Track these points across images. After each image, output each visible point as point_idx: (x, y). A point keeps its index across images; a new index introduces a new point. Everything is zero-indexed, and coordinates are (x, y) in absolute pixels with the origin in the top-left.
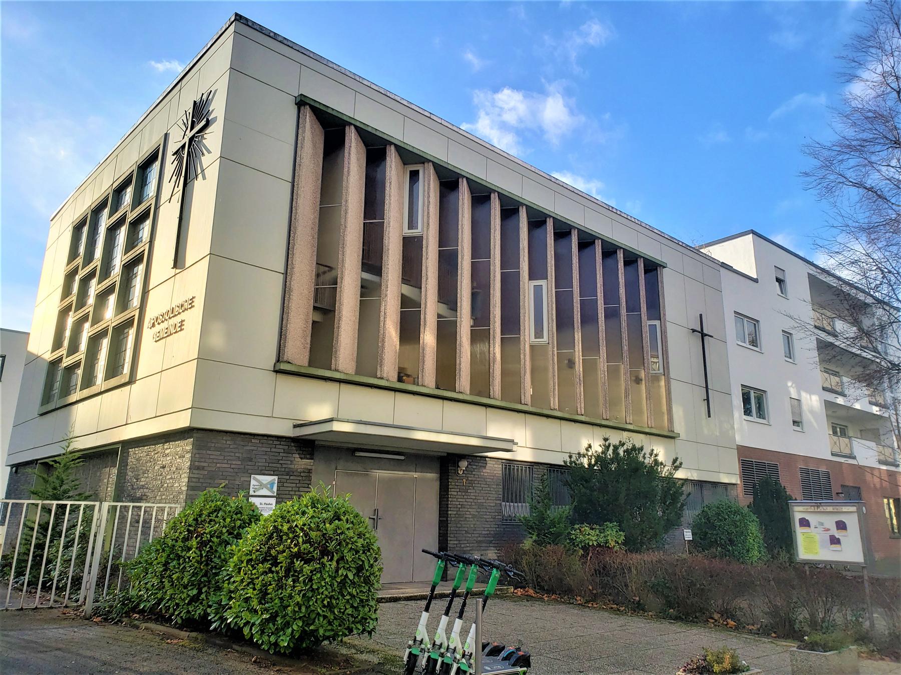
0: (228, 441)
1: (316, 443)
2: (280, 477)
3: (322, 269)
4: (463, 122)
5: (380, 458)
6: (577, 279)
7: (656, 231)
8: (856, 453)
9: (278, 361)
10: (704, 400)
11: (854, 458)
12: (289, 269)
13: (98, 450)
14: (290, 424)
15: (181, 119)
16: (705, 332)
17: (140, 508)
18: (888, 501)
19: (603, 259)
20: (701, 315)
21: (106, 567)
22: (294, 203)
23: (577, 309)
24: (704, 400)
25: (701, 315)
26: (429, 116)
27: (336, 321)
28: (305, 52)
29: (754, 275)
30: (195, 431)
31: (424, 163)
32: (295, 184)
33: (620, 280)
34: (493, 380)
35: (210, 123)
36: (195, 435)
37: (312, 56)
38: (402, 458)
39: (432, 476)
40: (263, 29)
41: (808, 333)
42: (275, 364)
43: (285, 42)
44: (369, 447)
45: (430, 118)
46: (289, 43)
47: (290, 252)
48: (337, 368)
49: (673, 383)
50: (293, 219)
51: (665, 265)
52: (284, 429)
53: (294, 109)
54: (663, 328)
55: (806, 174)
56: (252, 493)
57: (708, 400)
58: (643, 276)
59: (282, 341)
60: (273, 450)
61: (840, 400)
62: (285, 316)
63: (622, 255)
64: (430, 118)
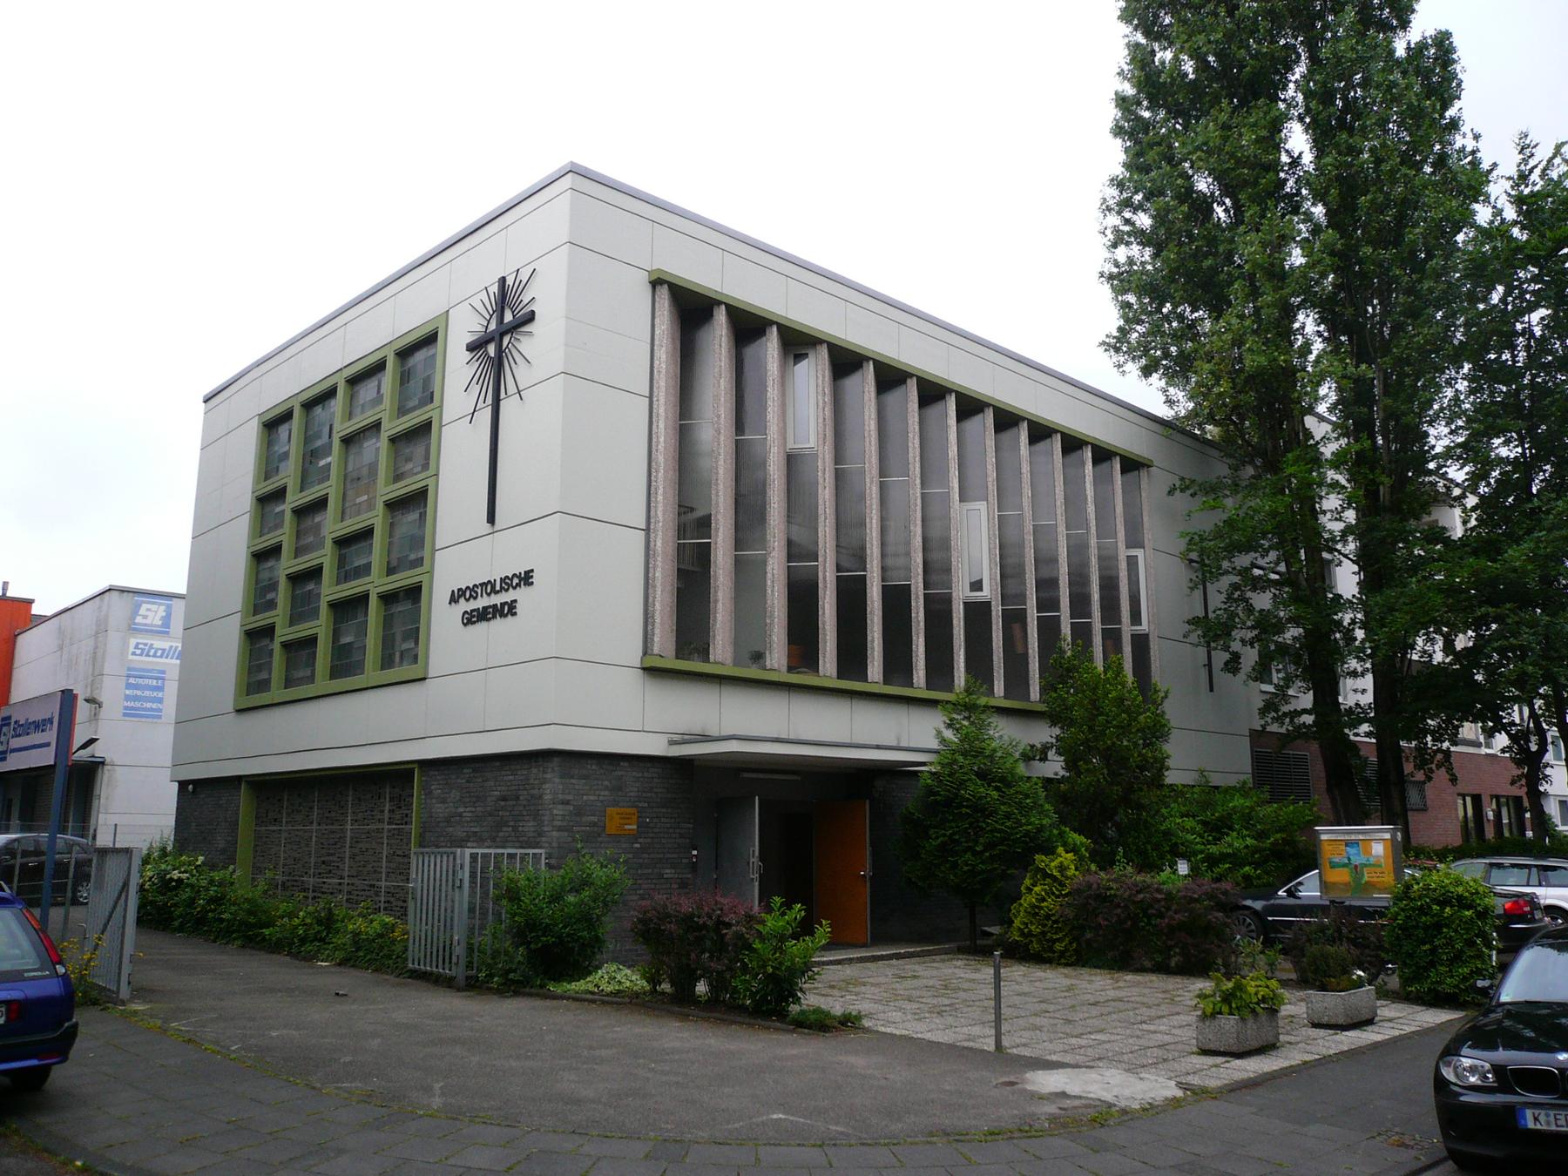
0: (593, 767)
3: (682, 510)
4: (1314, 306)
9: (645, 653)
14: (664, 739)
15: (497, 527)
18: (1464, 800)
19: (995, 432)
21: (476, 873)
22: (654, 427)
27: (712, 590)
30: (556, 760)
32: (655, 399)
33: (1088, 492)
47: (653, 499)
50: (654, 451)
51: (1149, 463)
53: (649, 288)
58: (1091, 467)
59: (650, 627)
60: (646, 774)
62: (650, 591)
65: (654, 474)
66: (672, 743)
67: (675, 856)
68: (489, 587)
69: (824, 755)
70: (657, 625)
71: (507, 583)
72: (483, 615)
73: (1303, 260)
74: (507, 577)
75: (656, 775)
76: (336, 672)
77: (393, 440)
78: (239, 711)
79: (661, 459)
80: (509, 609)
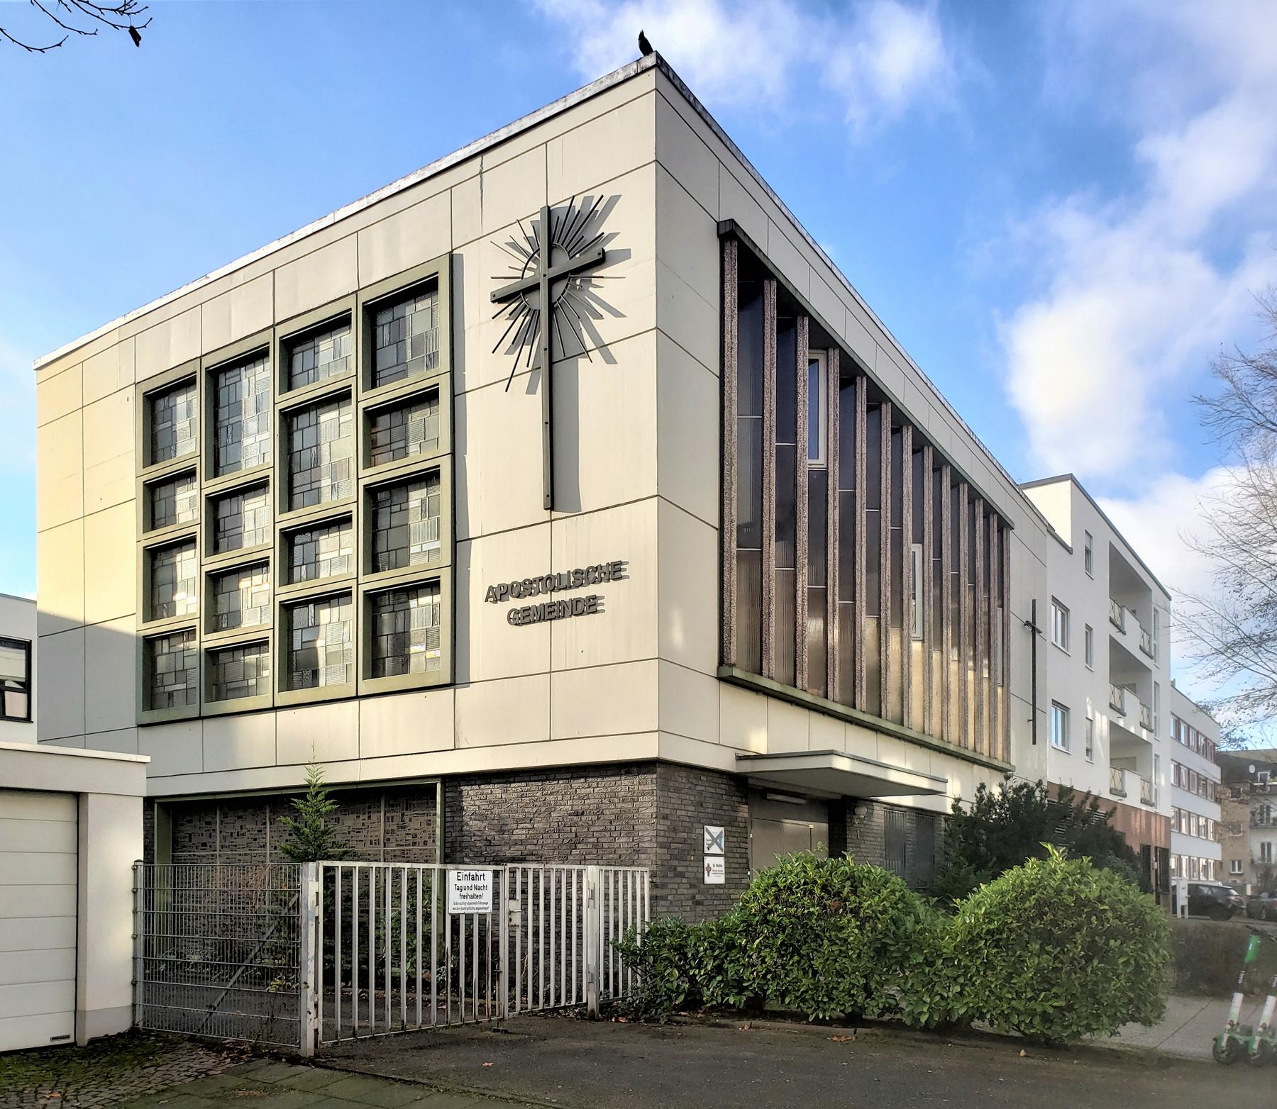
1: (751, 781)
2: (730, 829)
5: (789, 803)
6: (948, 544)
7: (1003, 473)
8: (1127, 790)
9: (721, 662)
10: (1029, 721)
11: (1125, 796)
12: (726, 523)
13: (359, 787)
16: (1038, 626)
17: (333, 869)
20: (1034, 601)
23: (948, 589)
24: (1029, 721)
25: (1034, 601)
26: (830, 265)
28: (723, 138)
29: (1068, 541)
31: (826, 349)
32: (726, 380)
34: (886, 693)
35: (607, 263)
36: (659, 770)
37: (728, 145)
38: (802, 801)
39: (819, 827)
40: (684, 88)
41: (1188, 635)
42: (718, 668)
43: (704, 115)
44: (791, 789)
45: (831, 269)
46: (708, 119)
47: (726, 495)
48: (770, 675)
49: (1013, 699)
52: (725, 762)
54: (1006, 619)
55: (1202, 400)
56: (706, 851)
57: (1034, 720)
59: (726, 635)
61: (1121, 723)
63: (982, 509)
64: (831, 269)
65: (726, 467)
66: (740, 758)
67: (737, 876)
68: (551, 582)
69: (1137, 571)
70: (734, 633)
71: (581, 577)
72: (550, 613)
73: (721, 880)
74: (528, 580)
75: (724, 792)
76: (287, 683)
77: (371, 416)
78: (140, 726)
79: (402, 383)
80: (590, 606)
